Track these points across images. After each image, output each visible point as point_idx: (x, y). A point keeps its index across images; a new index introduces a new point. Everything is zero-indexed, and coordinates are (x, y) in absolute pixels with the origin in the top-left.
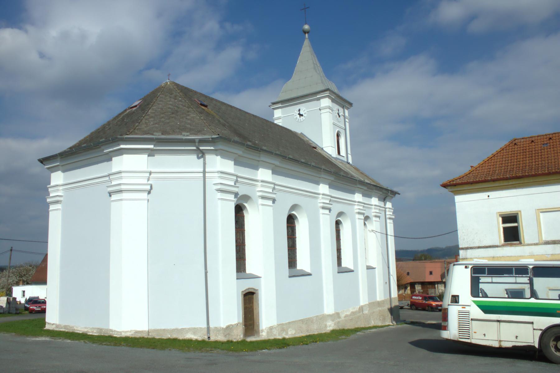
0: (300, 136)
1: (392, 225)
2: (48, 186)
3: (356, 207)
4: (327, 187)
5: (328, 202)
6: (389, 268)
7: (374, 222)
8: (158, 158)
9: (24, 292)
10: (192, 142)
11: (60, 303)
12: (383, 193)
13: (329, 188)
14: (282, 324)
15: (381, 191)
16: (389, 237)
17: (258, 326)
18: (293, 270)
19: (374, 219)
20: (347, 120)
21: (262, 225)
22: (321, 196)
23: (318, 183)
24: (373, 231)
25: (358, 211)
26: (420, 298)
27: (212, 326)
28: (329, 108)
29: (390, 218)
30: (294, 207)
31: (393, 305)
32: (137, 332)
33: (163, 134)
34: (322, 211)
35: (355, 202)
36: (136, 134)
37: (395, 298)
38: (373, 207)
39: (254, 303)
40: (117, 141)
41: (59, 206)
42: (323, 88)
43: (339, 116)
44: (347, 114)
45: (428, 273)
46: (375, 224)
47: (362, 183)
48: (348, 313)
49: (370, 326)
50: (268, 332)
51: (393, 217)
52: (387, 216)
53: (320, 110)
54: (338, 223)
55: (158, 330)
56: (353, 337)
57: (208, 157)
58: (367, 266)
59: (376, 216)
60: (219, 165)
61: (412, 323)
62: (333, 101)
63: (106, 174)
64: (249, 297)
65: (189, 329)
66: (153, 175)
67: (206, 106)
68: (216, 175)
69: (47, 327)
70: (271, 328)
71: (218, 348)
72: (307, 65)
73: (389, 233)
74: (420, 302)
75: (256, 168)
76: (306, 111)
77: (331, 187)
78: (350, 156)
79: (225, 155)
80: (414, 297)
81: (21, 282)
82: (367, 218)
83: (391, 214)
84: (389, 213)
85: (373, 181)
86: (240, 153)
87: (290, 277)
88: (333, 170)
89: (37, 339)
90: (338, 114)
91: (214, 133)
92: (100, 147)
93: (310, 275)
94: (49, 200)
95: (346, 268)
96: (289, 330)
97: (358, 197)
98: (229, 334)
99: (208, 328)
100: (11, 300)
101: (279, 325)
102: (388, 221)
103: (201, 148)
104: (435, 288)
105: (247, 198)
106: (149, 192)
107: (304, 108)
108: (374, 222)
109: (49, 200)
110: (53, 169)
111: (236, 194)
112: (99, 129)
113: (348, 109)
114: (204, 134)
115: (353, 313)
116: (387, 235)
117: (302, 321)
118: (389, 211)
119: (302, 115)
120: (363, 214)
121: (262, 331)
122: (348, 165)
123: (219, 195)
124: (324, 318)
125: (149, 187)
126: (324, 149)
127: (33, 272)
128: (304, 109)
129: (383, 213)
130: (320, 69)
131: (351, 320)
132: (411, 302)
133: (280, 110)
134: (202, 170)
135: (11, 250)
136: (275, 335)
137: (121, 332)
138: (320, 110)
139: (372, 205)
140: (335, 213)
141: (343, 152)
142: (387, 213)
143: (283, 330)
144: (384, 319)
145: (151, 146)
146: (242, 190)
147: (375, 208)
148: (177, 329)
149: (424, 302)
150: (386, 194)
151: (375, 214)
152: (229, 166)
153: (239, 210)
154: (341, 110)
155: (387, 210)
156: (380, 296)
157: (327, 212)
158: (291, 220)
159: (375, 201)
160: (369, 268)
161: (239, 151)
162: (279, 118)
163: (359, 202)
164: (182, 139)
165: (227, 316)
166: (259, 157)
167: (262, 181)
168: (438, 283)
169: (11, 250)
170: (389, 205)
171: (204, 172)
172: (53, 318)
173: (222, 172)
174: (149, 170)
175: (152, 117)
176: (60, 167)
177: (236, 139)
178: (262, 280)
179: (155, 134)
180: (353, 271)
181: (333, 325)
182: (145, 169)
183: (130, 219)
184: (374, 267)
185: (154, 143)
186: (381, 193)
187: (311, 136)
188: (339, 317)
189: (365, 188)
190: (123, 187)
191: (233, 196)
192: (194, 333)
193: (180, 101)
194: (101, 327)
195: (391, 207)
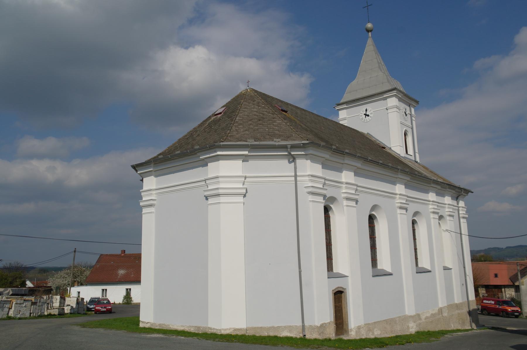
0: (368, 137)
1: (466, 224)
2: (141, 191)
3: (431, 207)
4: (403, 187)
5: (404, 202)
6: (464, 267)
7: (448, 221)
8: (252, 163)
9: (79, 293)
10: (284, 147)
11: (152, 300)
12: (456, 191)
13: (405, 188)
14: (369, 324)
15: (454, 190)
16: (463, 236)
17: (347, 325)
18: (330, 272)
19: (448, 218)
20: (413, 118)
21: (347, 225)
22: (398, 196)
23: (394, 184)
24: (447, 230)
25: (432, 210)
26: (493, 302)
27: (307, 324)
28: (397, 107)
29: (463, 218)
30: (375, 207)
31: (471, 309)
32: (235, 330)
33: (255, 141)
34: (399, 211)
35: (429, 201)
36: (230, 141)
37: (473, 301)
38: (447, 206)
39: (343, 302)
40: (215, 148)
41: (152, 209)
42: (390, 88)
43: (406, 115)
44: (413, 113)
45: (493, 275)
46: (449, 224)
47: (436, 182)
48: (428, 315)
49: (450, 329)
50: (356, 332)
51: (467, 216)
52: (461, 216)
53: (387, 109)
54: (414, 222)
55: (255, 328)
56: (442, 339)
57: (299, 161)
58: (444, 267)
59: (450, 216)
60: (309, 168)
61: (493, 328)
62: (400, 100)
63: (203, 179)
64: (339, 295)
65: (285, 327)
66: (247, 180)
67: (286, 112)
68: (307, 178)
69: (141, 325)
70: (359, 328)
71: (325, 346)
72: (372, 68)
73: (463, 233)
74: (493, 306)
75: (340, 171)
76: (372, 112)
77: (407, 186)
78: (417, 155)
79: (314, 159)
80: (485, 301)
81: (76, 283)
82: (441, 217)
83: (464, 213)
84: (462, 212)
85: (444, 180)
86: (327, 156)
87: (373, 276)
88: (407, 170)
89: (149, 336)
90: (405, 113)
91: (303, 139)
92: (196, 154)
93: (391, 274)
94: (141, 204)
95: (383, 270)
96: (375, 330)
97: (432, 196)
98: (323, 333)
99: (303, 326)
100: (80, 300)
101: (365, 325)
102: (462, 220)
103: (292, 153)
104: (502, 292)
105: (333, 199)
106: (245, 196)
107: (371, 108)
108: (448, 221)
109: (141, 204)
110: (148, 174)
111: (324, 196)
112: (186, 136)
113: (414, 107)
114: (294, 140)
115: (433, 315)
116: (461, 234)
117: (386, 321)
118: (462, 210)
119: (368, 116)
120: (438, 213)
121: (351, 330)
122: (416, 164)
123: (311, 198)
124: (405, 319)
125: (244, 191)
126: (392, 149)
127: (88, 273)
128: (370, 109)
129: (457, 212)
130: (385, 68)
131: (432, 322)
132: (482, 306)
133: (345, 110)
134: (293, 174)
135: (75, 251)
136: (363, 335)
137: (220, 330)
138: (387, 109)
139: (445, 204)
140: (411, 212)
141: (410, 152)
142: (460, 212)
143: (369, 330)
144: (463, 323)
145: (246, 153)
146: (329, 193)
147: (448, 208)
148: (273, 327)
149: (498, 306)
150: (459, 192)
151: (449, 213)
152: (317, 169)
153: (327, 210)
154: (408, 108)
155: (460, 209)
156: (458, 299)
157: (404, 211)
158: (372, 219)
159: (448, 200)
160: (446, 269)
161: (327, 155)
162: (344, 119)
163: (433, 201)
164: (275, 145)
165: (320, 316)
166: (343, 160)
167: (347, 183)
168: (505, 286)
169: (75, 251)
170: (462, 204)
171: (296, 176)
172: (147, 317)
173: (312, 176)
174: (244, 175)
175: (241, 124)
176: (153, 173)
177: (323, 144)
178: (350, 279)
179: (248, 140)
180: (430, 271)
181: (415, 327)
182: (240, 174)
183: (229, 221)
184: (450, 267)
185: (249, 149)
186: (454, 192)
187: (378, 135)
188: (420, 319)
189: (439, 187)
190: (221, 191)
191: (322, 198)
192: (290, 331)
193: (264, 108)
194: (199, 325)
195: (464, 206)
